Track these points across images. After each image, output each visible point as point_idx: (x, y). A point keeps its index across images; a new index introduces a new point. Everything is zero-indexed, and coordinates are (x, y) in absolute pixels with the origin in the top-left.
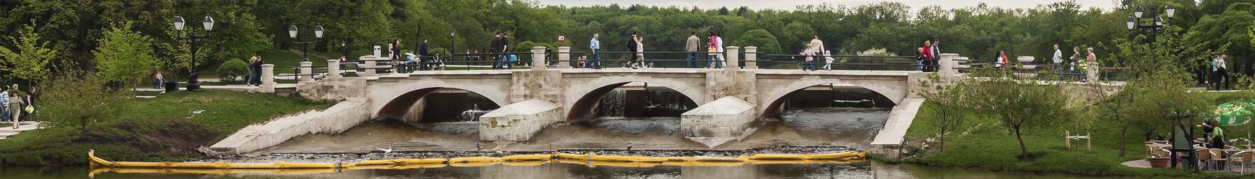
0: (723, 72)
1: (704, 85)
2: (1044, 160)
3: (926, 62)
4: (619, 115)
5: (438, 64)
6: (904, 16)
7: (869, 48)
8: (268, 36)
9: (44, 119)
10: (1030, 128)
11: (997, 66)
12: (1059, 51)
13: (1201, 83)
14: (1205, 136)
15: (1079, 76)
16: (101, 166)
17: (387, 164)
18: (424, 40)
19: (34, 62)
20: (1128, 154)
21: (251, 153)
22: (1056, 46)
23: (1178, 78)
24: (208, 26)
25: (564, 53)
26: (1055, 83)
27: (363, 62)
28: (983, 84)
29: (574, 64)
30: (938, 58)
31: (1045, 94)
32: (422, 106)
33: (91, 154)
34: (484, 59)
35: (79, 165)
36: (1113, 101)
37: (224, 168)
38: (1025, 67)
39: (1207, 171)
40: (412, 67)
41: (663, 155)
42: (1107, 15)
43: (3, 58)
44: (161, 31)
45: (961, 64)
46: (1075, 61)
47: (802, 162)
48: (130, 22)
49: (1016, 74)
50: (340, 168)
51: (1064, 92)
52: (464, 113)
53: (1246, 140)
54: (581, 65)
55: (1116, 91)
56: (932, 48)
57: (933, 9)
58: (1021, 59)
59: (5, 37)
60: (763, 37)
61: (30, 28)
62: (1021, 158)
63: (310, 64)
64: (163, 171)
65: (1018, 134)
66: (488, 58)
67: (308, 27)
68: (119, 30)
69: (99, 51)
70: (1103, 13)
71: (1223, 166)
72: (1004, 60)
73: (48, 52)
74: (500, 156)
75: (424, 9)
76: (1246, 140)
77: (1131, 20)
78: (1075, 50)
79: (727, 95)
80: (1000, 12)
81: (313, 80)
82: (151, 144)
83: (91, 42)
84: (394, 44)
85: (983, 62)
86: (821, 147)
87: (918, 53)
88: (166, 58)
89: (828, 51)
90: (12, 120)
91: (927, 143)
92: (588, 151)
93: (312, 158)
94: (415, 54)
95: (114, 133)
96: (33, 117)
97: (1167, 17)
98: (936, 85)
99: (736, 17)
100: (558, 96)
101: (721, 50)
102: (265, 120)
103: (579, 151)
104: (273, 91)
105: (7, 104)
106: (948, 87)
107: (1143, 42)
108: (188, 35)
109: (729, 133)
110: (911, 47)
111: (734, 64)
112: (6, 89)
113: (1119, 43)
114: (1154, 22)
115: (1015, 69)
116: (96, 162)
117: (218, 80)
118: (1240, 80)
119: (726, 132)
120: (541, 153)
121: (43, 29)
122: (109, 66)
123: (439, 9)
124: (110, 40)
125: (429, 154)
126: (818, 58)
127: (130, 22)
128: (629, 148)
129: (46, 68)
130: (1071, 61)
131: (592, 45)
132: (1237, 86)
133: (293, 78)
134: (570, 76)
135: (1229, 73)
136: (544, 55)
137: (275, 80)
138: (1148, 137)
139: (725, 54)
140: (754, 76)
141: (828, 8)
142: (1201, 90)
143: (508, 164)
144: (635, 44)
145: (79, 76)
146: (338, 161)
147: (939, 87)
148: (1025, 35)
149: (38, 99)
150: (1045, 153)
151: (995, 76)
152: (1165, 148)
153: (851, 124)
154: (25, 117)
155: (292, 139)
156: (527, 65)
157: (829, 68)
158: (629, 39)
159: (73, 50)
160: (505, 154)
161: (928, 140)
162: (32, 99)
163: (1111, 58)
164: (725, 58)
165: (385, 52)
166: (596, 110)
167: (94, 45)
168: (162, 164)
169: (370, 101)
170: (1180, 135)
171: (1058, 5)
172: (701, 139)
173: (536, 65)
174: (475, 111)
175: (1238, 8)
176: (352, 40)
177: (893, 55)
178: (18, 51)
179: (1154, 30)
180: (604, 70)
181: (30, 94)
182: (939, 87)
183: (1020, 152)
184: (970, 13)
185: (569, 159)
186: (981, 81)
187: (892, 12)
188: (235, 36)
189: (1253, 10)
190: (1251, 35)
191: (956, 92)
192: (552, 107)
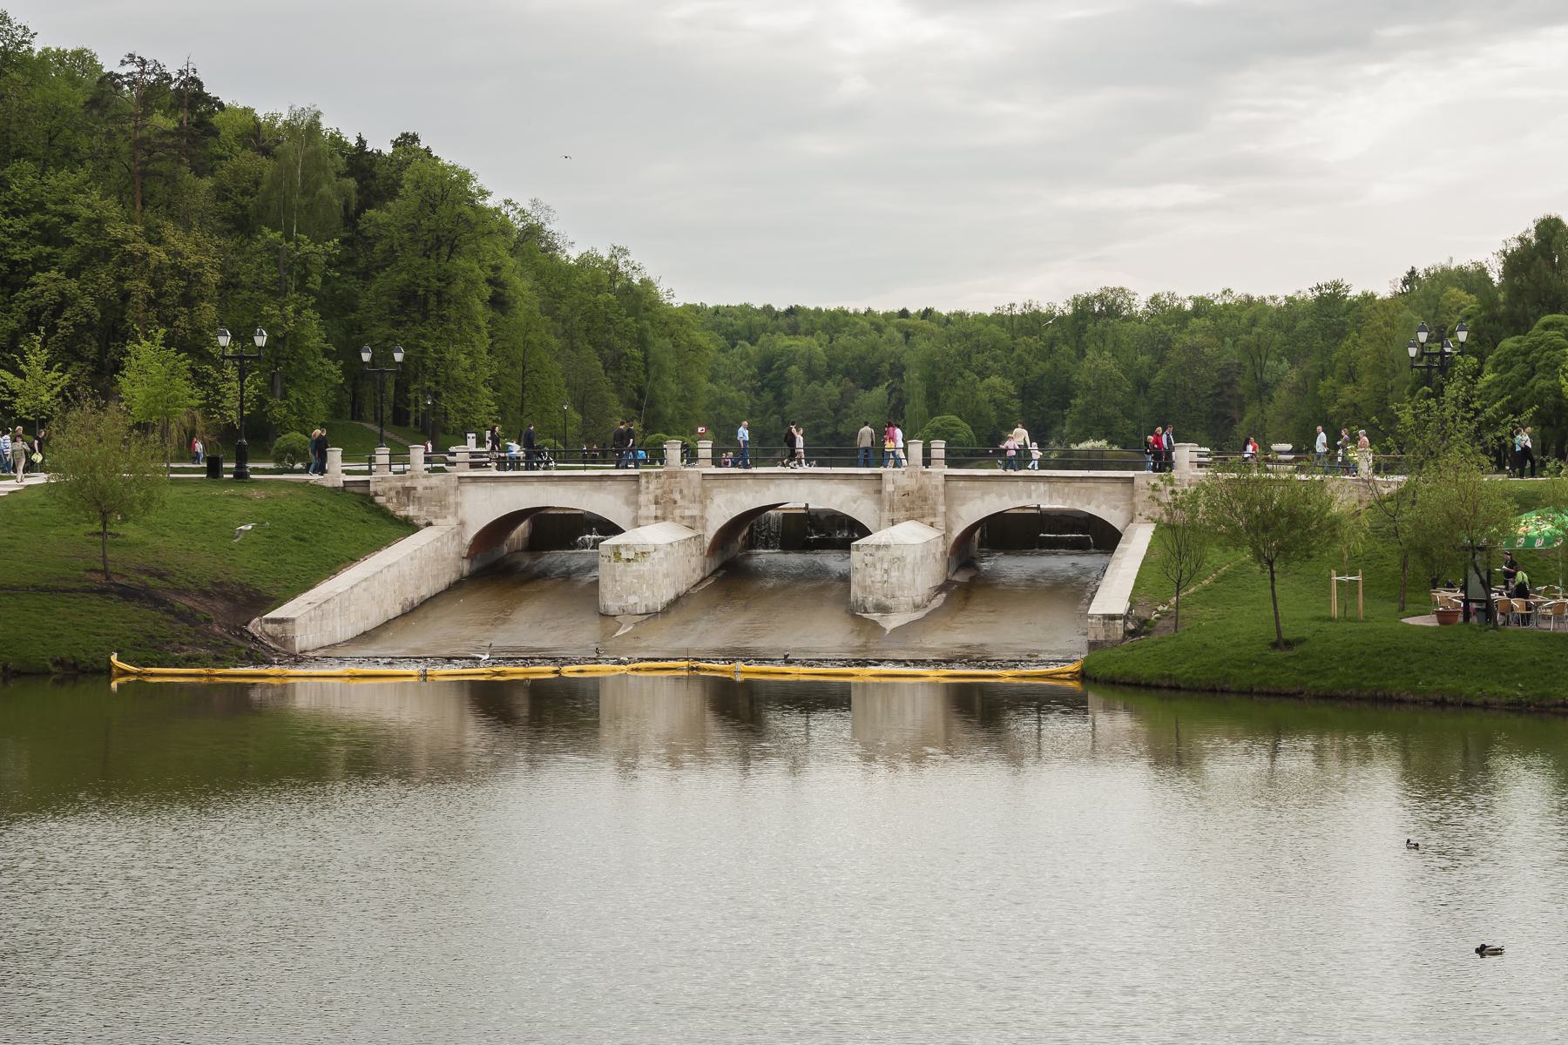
0: (903, 473)
1: (879, 492)
2: (1304, 648)
3: (1157, 457)
4: (773, 548)
5: (547, 462)
6: (1130, 305)
7: (1086, 439)
8: (335, 364)
9: (56, 470)
10: (1287, 564)
11: (1246, 456)
12: (1323, 434)
13: (1500, 469)
14: (1506, 583)
15: (1348, 469)
16: (126, 673)
17: (483, 674)
18: (530, 426)
19: (42, 389)
20: (1410, 608)
21: (313, 651)
22: (1320, 428)
23: (1472, 463)
24: (260, 341)
25: (705, 448)
26: (1318, 478)
27: (454, 454)
28: (1228, 481)
29: (717, 462)
30: (1171, 449)
31: (1305, 494)
32: (527, 530)
33: (114, 658)
34: (605, 456)
35: (99, 672)
36: (1390, 499)
37: (280, 676)
38: (1281, 457)
39: (1509, 627)
40: (514, 463)
41: (829, 665)
42: (1383, 301)
43: (4, 384)
44: (201, 348)
45: (1201, 456)
46: (1343, 448)
47: (1002, 681)
48: (162, 331)
49: (1269, 466)
50: (425, 676)
51: (1329, 492)
52: (580, 539)
53: (1556, 588)
54: (726, 464)
55: (1394, 487)
56: (1164, 436)
57: (1166, 295)
58: (1275, 447)
59: (6, 354)
60: (953, 425)
61: (38, 337)
62: (1275, 645)
63: (387, 450)
64: (204, 680)
65: (1272, 572)
66: (610, 455)
67: (385, 349)
68: (149, 344)
69: (124, 376)
70: (1378, 298)
71: (1528, 620)
72: (1254, 449)
73: (60, 377)
74: (625, 663)
75: (530, 290)
76: (1556, 588)
77: (1413, 346)
78: (1343, 433)
79: (908, 519)
80: (1250, 300)
81: (391, 474)
82: (189, 611)
83: (114, 361)
84: (493, 431)
85: (1229, 454)
86: (1025, 661)
87: (1147, 443)
88: (207, 388)
89: (1034, 444)
90: (15, 472)
91: (1158, 612)
92: (734, 661)
93: (390, 663)
94: (518, 443)
95: (143, 582)
96: (42, 468)
97: (1458, 341)
98: (1170, 488)
99: (919, 322)
100: (698, 518)
101: (901, 444)
102: (331, 574)
103: (723, 660)
104: (342, 484)
105: (9, 452)
106: (1185, 492)
107: (1428, 396)
108: (235, 352)
109: (911, 605)
110: (1137, 433)
111: (917, 463)
112: (8, 432)
113: (1398, 410)
114: (1442, 347)
115: (1268, 461)
116: (120, 668)
117: (271, 465)
118: (1549, 466)
119: (908, 604)
120: (676, 659)
121: (53, 338)
122: (137, 395)
123: (549, 291)
124: (137, 359)
125: (536, 661)
126: (1022, 452)
127: (162, 331)
128: (786, 656)
129: (57, 396)
130: (1337, 448)
131: (740, 435)
132: (1545, 473)
133: (367, 468)
134: (712, 477)
135: (1535, 457)
136: (679, 452)
137: (343, 471)
138: (1435, 584)
139: (905, 450)
140: (942, 478)
141: (1034, 306)
142: (1500, 478)
143: (635, 673)
144: (794, 438)
145: (98, 408)
146: (422, 667)
147: (1173, 492)
148: (1281, 361)
149: (48, 445)
150: (1305, 640)
151: (1242, 472)
152: (1455, 598)
153: (1063, 571)
154: (31, 467)
155: (365, 633)
156: (658, 464)
157: (1036, 468)
158: (786, 431)
159: (91, 374)
160: (631, 661)
161: (1160, 608)
162: (40, 445)
163: (1389, 443)
164: (906, 455)
165: (481, 442)
166: (744, 538)
167: (118, 367)
168: (203, 671)
169: (462, 524)
170: (1474, 582)
171: (1321, 289)
172: (875, 616)
173: (670, 463)
174: (594, 536)
175: (1547, 327)
176: (440, 394)
177: (1115, 448)
178: (22, 375)
179: (1442, 358)
180: (754, 470)
181: (37, 438)
182: (1173, 492)
183: (1275, 638)
184: (1212, 302)
185: (711, 670)
186: (1225, 478)
187: (1114, 300)
188: (293, 360)
189: (1566, 330)
190: (1563, 381)
191: (1194, 498)
192: (690, 534)
